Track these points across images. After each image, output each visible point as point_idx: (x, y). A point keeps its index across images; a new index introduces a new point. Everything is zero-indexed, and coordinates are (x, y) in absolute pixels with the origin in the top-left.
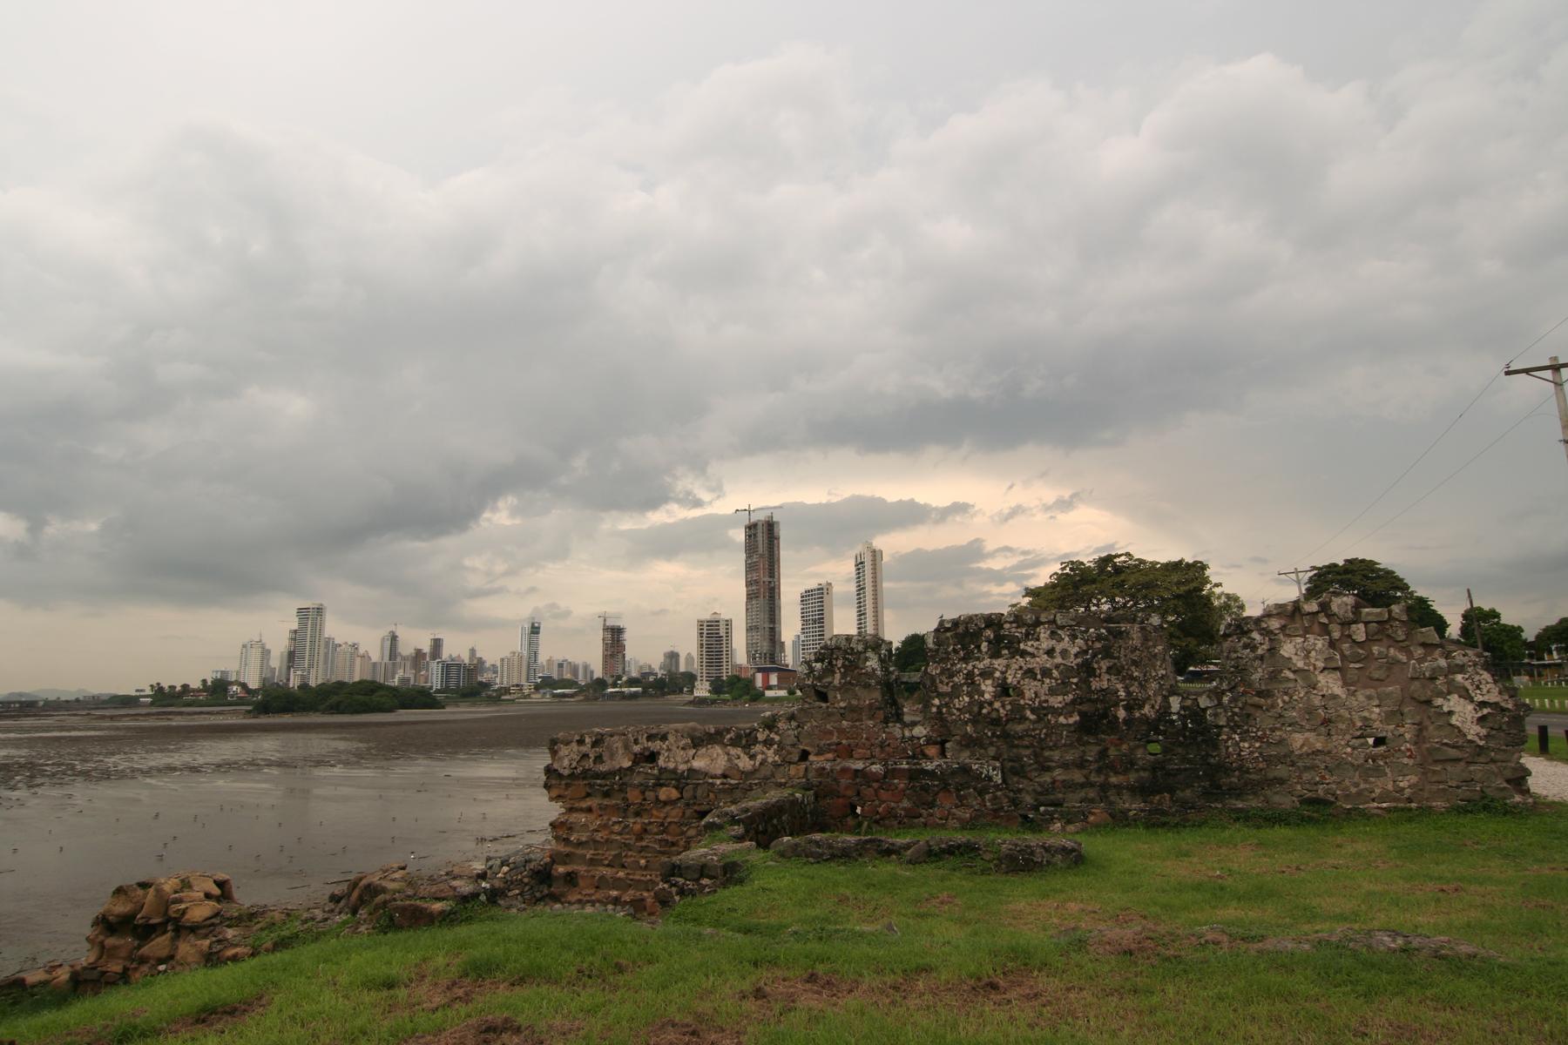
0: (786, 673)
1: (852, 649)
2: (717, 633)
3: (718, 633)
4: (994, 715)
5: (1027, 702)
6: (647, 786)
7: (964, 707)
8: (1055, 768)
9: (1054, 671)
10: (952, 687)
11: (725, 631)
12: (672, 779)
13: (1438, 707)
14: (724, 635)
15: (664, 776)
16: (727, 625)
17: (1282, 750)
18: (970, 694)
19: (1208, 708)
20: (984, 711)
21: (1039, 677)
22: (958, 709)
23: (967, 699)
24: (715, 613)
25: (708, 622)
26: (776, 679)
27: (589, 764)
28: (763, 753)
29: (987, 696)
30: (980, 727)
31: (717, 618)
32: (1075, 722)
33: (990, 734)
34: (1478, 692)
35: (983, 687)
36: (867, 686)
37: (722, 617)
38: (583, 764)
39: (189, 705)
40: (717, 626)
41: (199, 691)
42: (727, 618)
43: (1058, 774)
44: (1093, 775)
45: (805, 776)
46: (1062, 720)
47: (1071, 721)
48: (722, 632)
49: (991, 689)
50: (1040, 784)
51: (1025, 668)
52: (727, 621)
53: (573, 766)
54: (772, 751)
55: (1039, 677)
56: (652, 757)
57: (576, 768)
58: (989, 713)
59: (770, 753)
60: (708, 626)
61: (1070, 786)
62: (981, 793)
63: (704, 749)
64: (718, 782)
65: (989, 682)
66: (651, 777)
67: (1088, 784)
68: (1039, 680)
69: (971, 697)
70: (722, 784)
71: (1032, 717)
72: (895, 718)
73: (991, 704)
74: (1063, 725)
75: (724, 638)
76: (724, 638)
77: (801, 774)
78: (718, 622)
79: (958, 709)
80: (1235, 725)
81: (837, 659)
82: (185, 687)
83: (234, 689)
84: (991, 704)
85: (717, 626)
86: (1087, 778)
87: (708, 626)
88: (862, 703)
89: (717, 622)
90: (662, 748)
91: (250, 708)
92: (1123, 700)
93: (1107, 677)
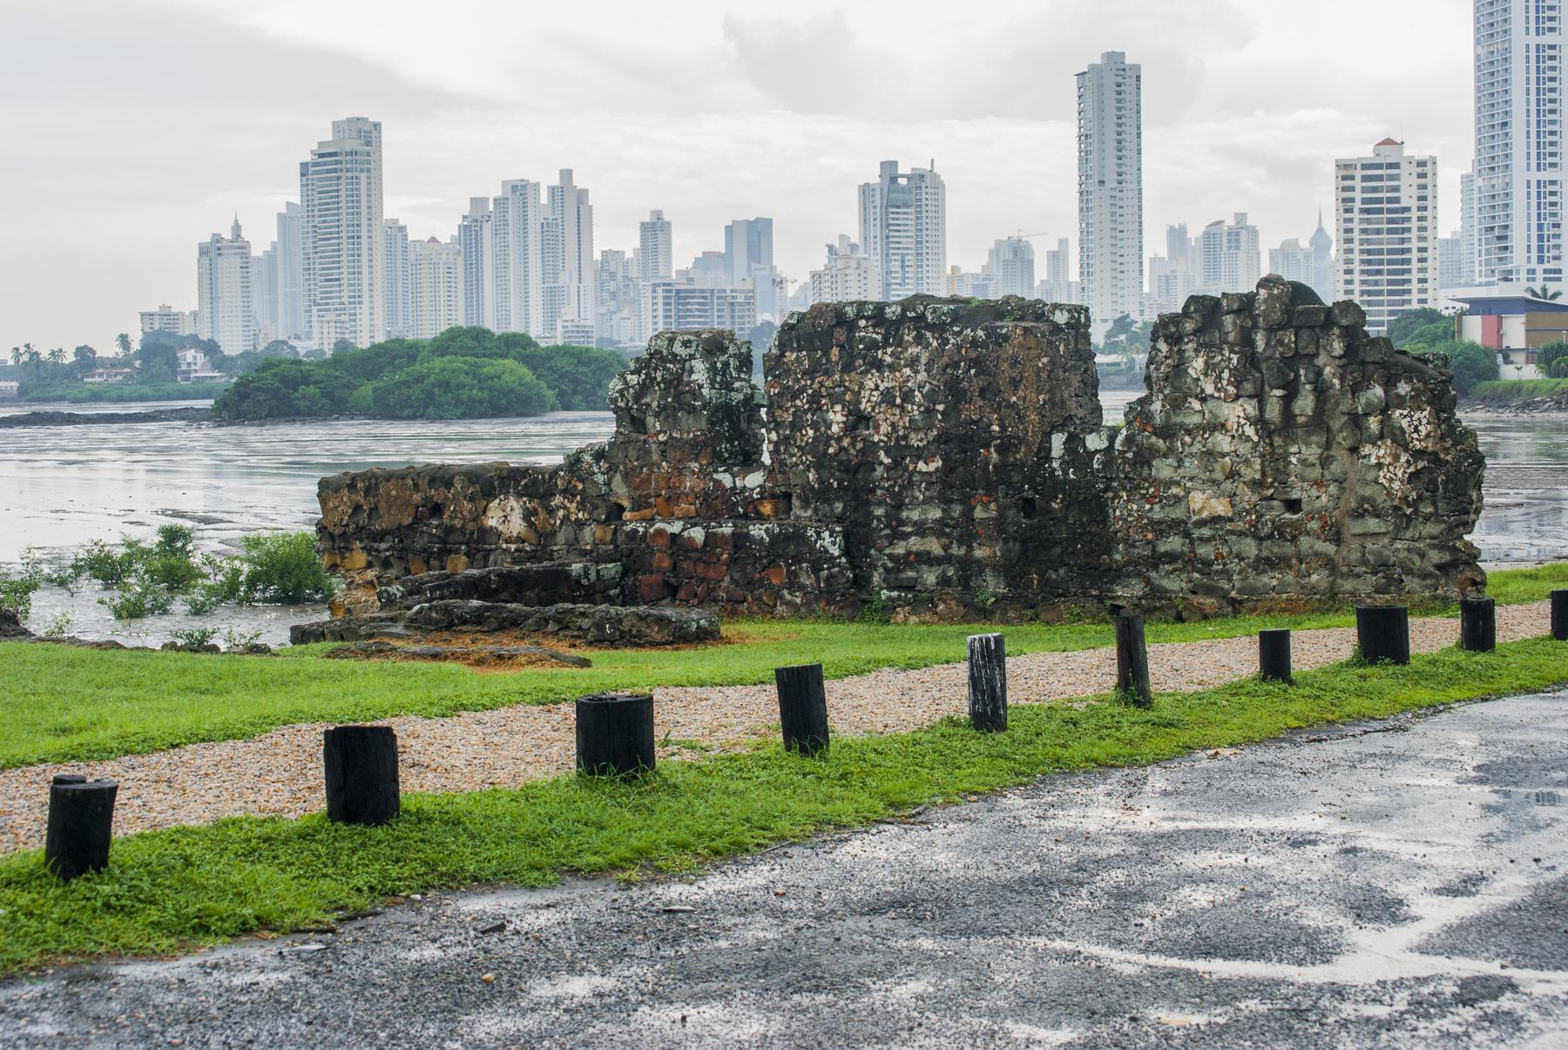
0: (1555, 315)
1: (675, 355)
2: (1390, 200)
3: (1397, 200)
4: (843, 457)
5: (882, 437)
6: (432, 553)
7: (807, 443)
8: (910, 535)
9: (916, 393)
10: (794, 414)
11: (1415, 192)
12: (462, 543)
13: (1364, 457)
14: (1414, 204)
15: (451, 538)
16: (1422, 175)
17: (1178, 513)
18: (815, 426)
19: (1097, 451)
20: (831, 450)
21: (898, 401)
22: (799, 448)
23: (811, 432)
24: (1388, 142)
25: (1364, 167)
26: (1522, 329)
27: (363, 519)
28: (565, 508)
29: (835, 429)
30: (825, 474)
31: (1389, 155)
32: (937, 469)
33: (835, 485)
34: (1415, 436)
35: (831, 416)
36: (692, 410)
37: (1408, 152)
38: (355, 519)
39: (97, 397)
40: (1391, 177)
41: (113, 364)
42: (1421, 155)
43: (915, 543)
44: (955, 545)
45: (614, 541)
46: (921, 466)
47: (932, 467)
48: (1408, 197)
49: (840, 418)
50: (891, 557)
51: (881, 388)
52: (1421, 164)
53: (345, 522)
54: (574, 505)
55: (898, 401)
56: (437, 510)
57: (347, 525)
58: (836, 454)
59: (573, 507)
60: (1364, 178)
61: (925, 558)
62: (816, 570)
63: (497, 501)
64: (513, 547)
65: (838, 408)
66: (436, 540)
67: (947, 559)
68: (898, 406)
69: (816, 430)
70: (516, 550)
71: (887, 461)
72: (741, 458)
73: (839, 440)
74: (920, 473)
75: (1414, 214)
76: (1414, 214)
77: (609, 538)
78: (1396, 166)
79: (799, 448)
80: (1126, 478)
81: (655, 369)
82: (84, 353)
83: (190, 359)
84: (839, 440)
85: (1391, 177)
86: (945, 550)
87: (1364, 178)
88: (685, 436)
89: (1391, 166)
90: (447, 498)
91: (208, 403)
92: (998, 438)
93: (980, 403)
